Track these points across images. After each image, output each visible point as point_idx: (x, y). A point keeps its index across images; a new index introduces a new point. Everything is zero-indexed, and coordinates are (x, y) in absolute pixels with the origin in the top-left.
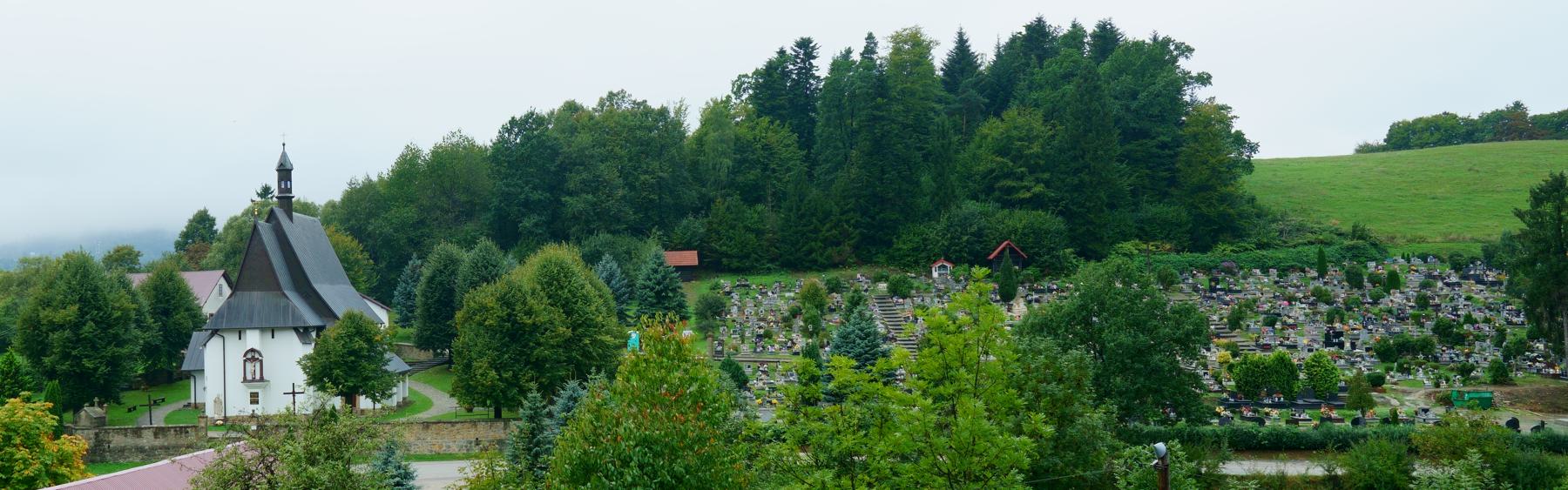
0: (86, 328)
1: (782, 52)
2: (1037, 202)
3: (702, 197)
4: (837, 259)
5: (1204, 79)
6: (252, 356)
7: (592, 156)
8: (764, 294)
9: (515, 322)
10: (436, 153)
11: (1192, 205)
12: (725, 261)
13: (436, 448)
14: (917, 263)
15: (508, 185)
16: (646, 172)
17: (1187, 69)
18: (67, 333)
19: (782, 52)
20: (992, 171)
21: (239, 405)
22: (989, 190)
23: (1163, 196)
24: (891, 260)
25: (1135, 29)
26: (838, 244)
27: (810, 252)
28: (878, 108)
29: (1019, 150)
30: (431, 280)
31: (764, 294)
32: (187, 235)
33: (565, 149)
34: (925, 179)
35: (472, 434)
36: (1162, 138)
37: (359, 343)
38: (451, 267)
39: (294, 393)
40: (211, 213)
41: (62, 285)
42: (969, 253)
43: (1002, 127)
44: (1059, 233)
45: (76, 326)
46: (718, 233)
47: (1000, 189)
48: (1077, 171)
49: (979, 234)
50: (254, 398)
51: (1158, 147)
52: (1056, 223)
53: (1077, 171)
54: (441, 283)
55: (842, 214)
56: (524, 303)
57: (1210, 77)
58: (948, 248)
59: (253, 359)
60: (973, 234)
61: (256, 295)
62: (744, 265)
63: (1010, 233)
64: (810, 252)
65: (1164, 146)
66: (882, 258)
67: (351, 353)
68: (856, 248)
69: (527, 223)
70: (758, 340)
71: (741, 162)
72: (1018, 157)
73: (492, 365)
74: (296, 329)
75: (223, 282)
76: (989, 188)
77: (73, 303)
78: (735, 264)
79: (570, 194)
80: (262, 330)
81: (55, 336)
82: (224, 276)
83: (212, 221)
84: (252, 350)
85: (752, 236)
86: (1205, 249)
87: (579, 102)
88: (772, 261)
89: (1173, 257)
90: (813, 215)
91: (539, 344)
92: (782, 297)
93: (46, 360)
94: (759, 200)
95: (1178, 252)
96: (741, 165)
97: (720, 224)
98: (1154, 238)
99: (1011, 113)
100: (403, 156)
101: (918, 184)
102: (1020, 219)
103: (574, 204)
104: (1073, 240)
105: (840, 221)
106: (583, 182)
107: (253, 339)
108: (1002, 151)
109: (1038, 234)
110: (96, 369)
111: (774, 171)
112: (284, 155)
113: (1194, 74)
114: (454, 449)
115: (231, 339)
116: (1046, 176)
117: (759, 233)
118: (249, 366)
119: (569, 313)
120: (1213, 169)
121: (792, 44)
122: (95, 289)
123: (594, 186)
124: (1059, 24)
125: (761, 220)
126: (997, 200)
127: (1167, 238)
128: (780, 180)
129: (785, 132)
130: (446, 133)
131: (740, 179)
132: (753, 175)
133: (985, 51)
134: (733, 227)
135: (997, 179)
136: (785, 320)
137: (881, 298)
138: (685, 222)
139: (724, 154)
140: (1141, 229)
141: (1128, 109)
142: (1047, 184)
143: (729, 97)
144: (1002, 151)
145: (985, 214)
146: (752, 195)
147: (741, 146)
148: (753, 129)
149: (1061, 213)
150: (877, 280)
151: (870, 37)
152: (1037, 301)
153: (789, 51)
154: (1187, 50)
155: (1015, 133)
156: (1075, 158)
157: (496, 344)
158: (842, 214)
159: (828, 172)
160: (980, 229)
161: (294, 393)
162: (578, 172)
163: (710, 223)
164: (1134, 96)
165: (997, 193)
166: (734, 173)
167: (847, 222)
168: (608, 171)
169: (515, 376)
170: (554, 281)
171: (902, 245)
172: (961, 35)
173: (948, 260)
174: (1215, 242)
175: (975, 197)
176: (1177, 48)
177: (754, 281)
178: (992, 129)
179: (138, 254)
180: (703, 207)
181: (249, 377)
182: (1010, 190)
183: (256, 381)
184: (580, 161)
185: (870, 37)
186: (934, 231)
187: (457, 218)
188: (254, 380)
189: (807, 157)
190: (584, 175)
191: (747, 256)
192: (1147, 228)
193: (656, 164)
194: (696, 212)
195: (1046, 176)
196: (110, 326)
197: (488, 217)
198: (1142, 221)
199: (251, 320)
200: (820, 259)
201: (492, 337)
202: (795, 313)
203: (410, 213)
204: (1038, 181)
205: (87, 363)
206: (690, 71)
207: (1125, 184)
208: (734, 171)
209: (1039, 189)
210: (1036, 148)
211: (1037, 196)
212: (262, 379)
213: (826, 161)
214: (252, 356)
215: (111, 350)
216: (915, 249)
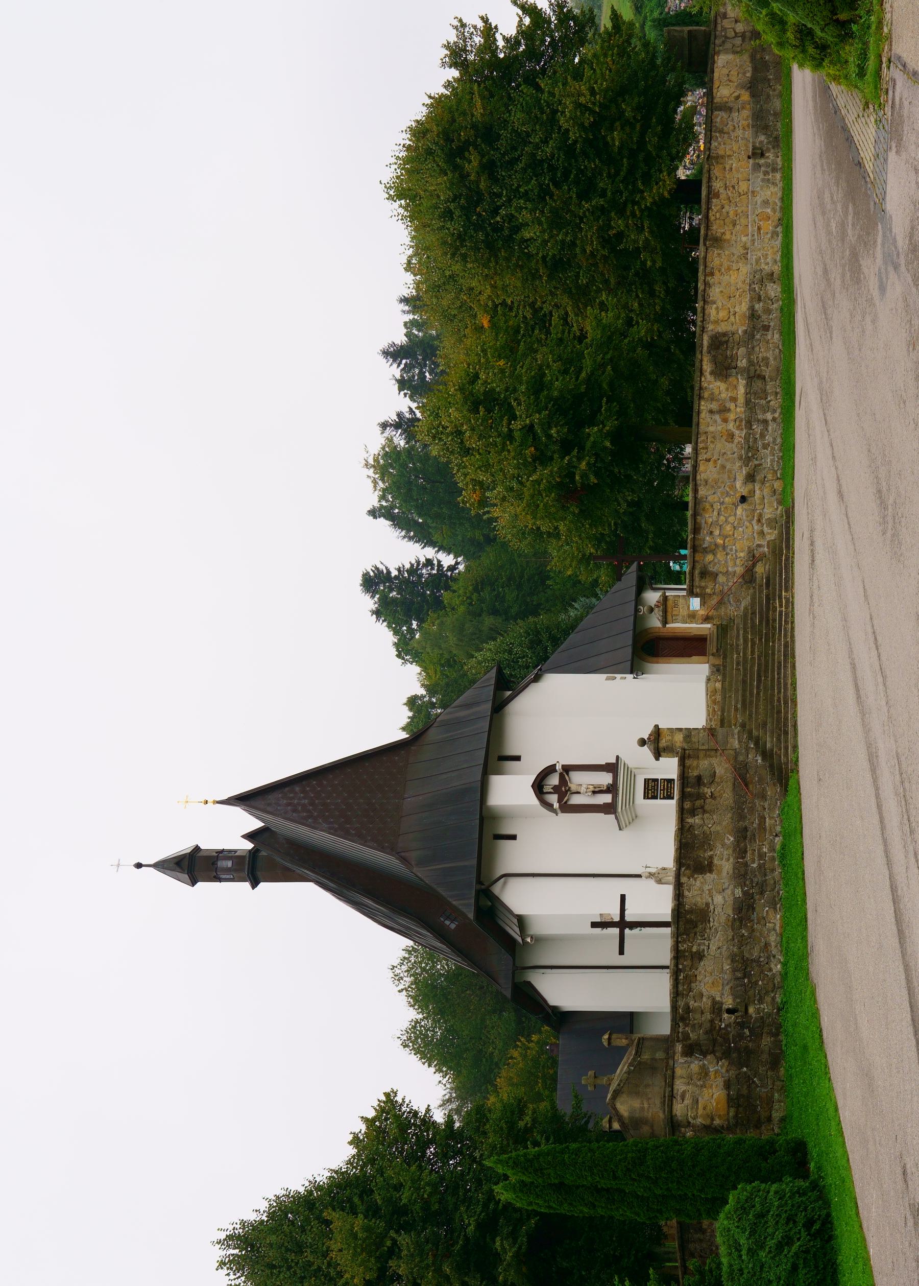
13: (768, 226)
59: (563, 790)
114: (772, 193)
212: (612, 768)
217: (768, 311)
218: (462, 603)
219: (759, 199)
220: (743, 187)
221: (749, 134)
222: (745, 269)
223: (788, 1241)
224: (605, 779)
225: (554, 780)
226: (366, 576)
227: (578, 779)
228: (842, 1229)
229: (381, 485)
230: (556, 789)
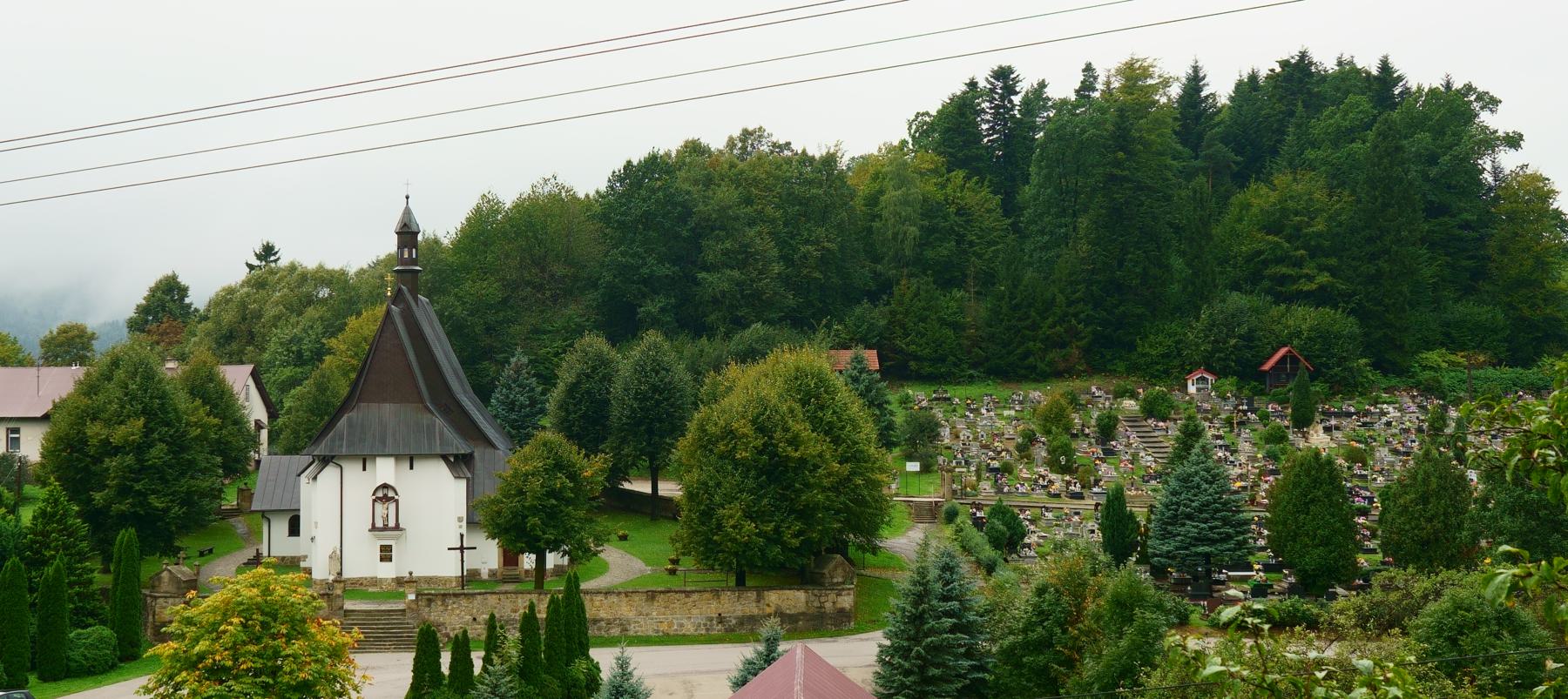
0: (154, 452)
1: (973, 85)
2: (1321, 298)
3: (876, 275)
4: (1062, 366)
5: (1514, 141)
6: (385, 494)
7: (737, 218)
8: (976, 411)
9: (774, 455)
10: (518, 206)
11: (1510, 305)
12: (913, 365)
13: (664, 627)
14: (1167, 373)
15: (623, 254)
16: (807, 242)
17: (1492, 127)
18: (130, 459)
19: (973, 85)
20: (1260, 253)
21: (362, 563)
22: (1255, 278)
23: (1467, 291)
24: (1133, 369)
25: (1421, 72)
26: (1063, 345)
27: (1026, 355)
28: (1118, 164)
29: (1298, 228)
30: (572, 389)
31: (976, 411)
32: (144, 310)
33: (701, 207)
34: (1177, 263)
35: (712, 608)
36: (1466, 216)
37: (561, 481)
38: (602, 371)
39: (462, 549)
40: (183, 280)
41: (113, 390)
42: (1237, 362)
43: (1274, 197)
44: (1352, 337)
45: (140, 449)
46: (903, 326)
47: (1272, 278)
48: (1373, 257)
49: (1249, 338)
50: (386, 554)
51: (1461, 227)
52: (1347, 325)
53: (1373, 257)
54: (588, 392)
55: (1070, 304)
56: (786, 430)
57: (1521, 136)
58: (1212, 354)
59: (386, 499)
60: (1241, 337)
61: (388, 408)
62: (939, 370)
63: (1291, 336)
64: (1026, 355)
65: (1466, 226)
66: (1121, 366)
67: (552, 493)
68: (1087, 351)
69: (651, 307)
70: (1003, 484)
71: (930, 230)
72: (1295, 236)
73: (748, 516)
74: (445, 458)
75: (251, 382)
76: (1253, 275)
77: (137, 415)
78: (927, 369)
79: (706, 268)
80: (398, 458)
81: (112, 463)
82: (255, 375)
83: (183, 291)
84: (385, 486)
85: (949, 332)
86: (1527, 364)
87: (704, 141)
88: (974, 366)
89: (1490, 371)
90: (1030, 305)
91: (808, 486)
92: (1000, 416)
93: (98, 497)
94: (960, 283)
95: (1494, 366)
96: (930, 234)
97: (907, 313)
98: (1462, 347)
99: (1282, 179)
100: (478, 210)
101: (1167, 268)
102: (1304, 317)
103: (716, 282)
104: (1368, 348)
105: (1066, 314)
106: (726, 253)
107: (385, 470)
108: (1273, 228)
109: (1324, 337)
110: (166, 510)
111: (971, 244)
112: (407, 212)
113: (1501, 133)
114: (689, 628)
115: (352, 470)
116: (1333, 261)
117: (956, 326)
118: (379, 506)
119: (836, 441)
120: (1537, 258)
121: (987, 73)
122: (163, 396)
123: (743, 257)
124: (1326, 60)
125: (961, 310)
126: (1268, 292)
127: (1480, 347)
128: (979, 256)
129: (985, 192)
130: (536, 179)
131: (929, 254)
132: (946, 249)
133: (1221, 87)
134: (923, 320)
135: (1265, 263)
136: (1020, 448)
137: (1132, 420)
138: (858, 311)
139: (907, 219)
140: (1447, 335)
141: (1426, 178)
142: (1333, 272)
143: (904, 143)
144: (1273, 228)
145: (1256, 311)
146: (948, 277)
147: (930, 210)
148: (943, 187)
149: (1352, 312)
150: (1120, 394)
151: (1088, 68)
152: (1337, 428)
153: (982, 84)
154: (1491, 103)
155: (1291, 204)
156: (1370, 240)
157: (750, 483)
158: (1070, 304)
159: (1045, 248)
160: (1251, 331)
161: (462, 549)
162: (718, 240)
163: (893, 313)
164: (1433, 160)
165: (1266, 283)
166: (920, 246)
167: (1076, 315)
168: (760, 240)
169: (777, 530)
170: (811, 394)
171: (1152, 347)
172: (1196, 69)
173: (1210, 370)
174: (1539, 355)
175: (1236, 287)
176: (1480, 97)
177: (957, 393)
178: (1260, 197)
179: (93, 337)
180: (881, 290)
181: (379, 524)
182: (1282, 280)
183: (387, 531)
184: (721, 224)
185: (1088, 68)
186: (1194, 333)
187: (555, 298)
188: (386, 528)
189: (1015, 227)
190: (728, 245)
191: (943, 360)
192: (1454, 333)
193: (820, 232)
194: (873, 297)
195: (1333, 261)
196: (183, 449)
197: (592, 297)
198: (1448, 325)
199: (383, 442)
200: (1041, 366)
201: (745, 475)
202: (1030, 439)
203: (490, 289)
204: (1321, 268)
205: (156, 502)
206: (855, 108)
207: (1427, 272)
208: (922, 244)
209: (1324, 278)
210: (1319, 226)
211: (1322, 288)
212: (397, 527)
213: (1042, 232)
214: (385, 494)
215: (185, 484)
216: (1165, 356)
217: (599, 629)
218: (946, 196)
219: (684, 621)
220: (695, 611)
221: (739, 613)
222: (631, 615)
223: (86, 658)
224: (392, 524)
225: (391, 494)
226: (1010, 70)
227: (392, 506)
228: (89, 681)
229: (892, 194)
230: (385, 496)
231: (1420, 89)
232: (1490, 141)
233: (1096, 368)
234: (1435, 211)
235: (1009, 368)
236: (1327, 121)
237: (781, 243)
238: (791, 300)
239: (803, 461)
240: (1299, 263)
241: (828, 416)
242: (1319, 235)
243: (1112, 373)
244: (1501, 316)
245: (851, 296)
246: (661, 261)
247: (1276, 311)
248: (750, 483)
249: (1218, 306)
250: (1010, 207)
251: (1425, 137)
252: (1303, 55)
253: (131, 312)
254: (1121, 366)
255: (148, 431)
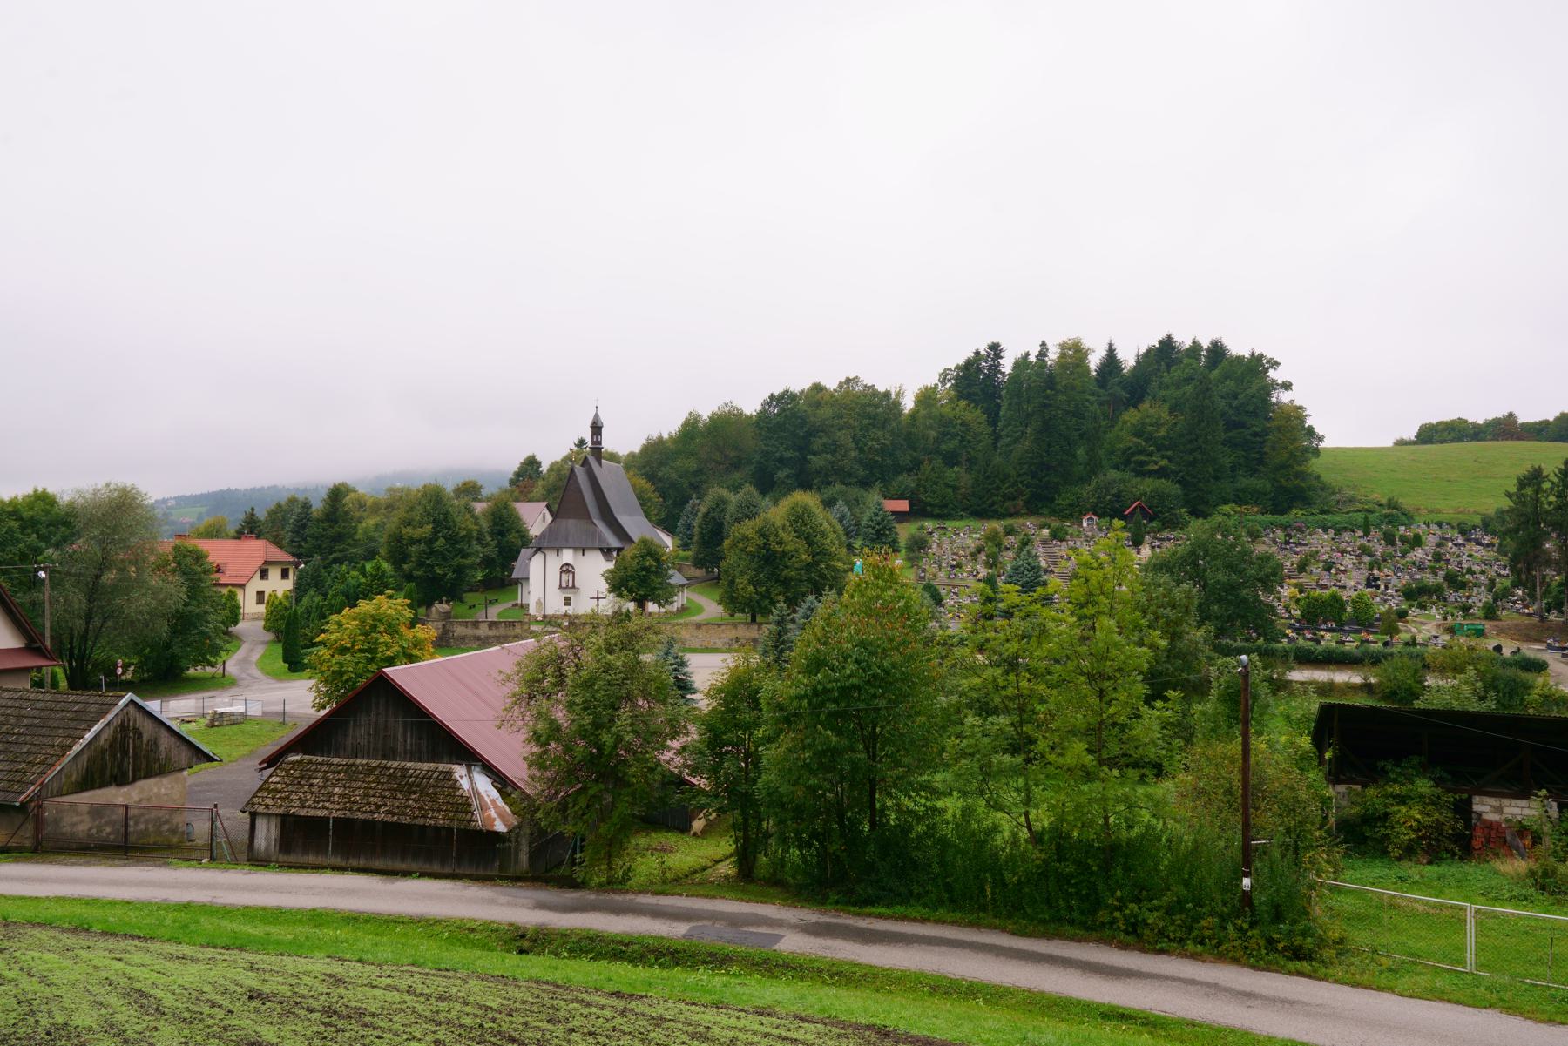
1: (977, 353)
2: (1162, 473)
5: (1287, 386)
6: (567, 569)
18: (423, 546)
19: (977, 353)
21: (555, 606)
22: (1127, 462)
23: (1253, 472)
24: (1053, 512)
25: (1238, 348)
27: (993, 503)
28: (1047, 397)
30: (706, 515)
32: (517, 474)
37: (650, 562)
40: (538, 458)
43: (1139, 415)
44: (1177, 497)
45: (430, 541)
48: (1192, 451)
49: (1118, 496)
50: (567, 601)
52: (1176, 489)
53: (1192, 451)
59: (568, 571)
61: (571, 521)
64: (993, 503)
65: (1256, 434)
66: (1046, 511)
67: (644, 569)
68: (1027, 502)
71: (944, 434)
73: (751, 582)
74: (601, 550)
78: (937, 511)
80: (575, 549)
81: (413, 548)
83: (539, 464)
86: (1282, 513)
89: (1259, 517)
94: (958, 464)
100: (687, 421)
101: (1074, 456)
102: (1149, 485)
103: (817, 462)
106: (824, 445)
107: (568, 556)
112: (597, 415)
114: (719, 644)
115: (551, 555)
116: (1169, 453)
117: (955, 488)
119: (810, 544)
122: (447, 513)
123: (834, 448)
124: (1184, 340)
127: (1256, 503)
130: (721, 404)
133: (1128, 359)
135: (1133, 454)
136: (972, 555)
137: (1044, 541)
145: (1123, 481)
146: (951, 460)
149: (1179, 482)
150: (1042, 527)
151: (1043, 344)
156: (1191, 441)
157: (754, 565)
164: (1236, 397)
168: (844, 437)
170: (800, 519)
171: (1062, 502)
172: (1111, 345)
173: (1095, 513)
174: (1290, 508)
175: (1116, 467)
178: (1131, 417)
180: (914, 467)
182: (1142, 463)
185: (1043, 344)
186: (1087, 492)
191: (946, 506)
193: (880, 434)
194: (909, 470)
195: (1169, 453)
196: (457, 542)
202: (980, 550)
203: (692, 465)
204: (1163, 457)
205: (438, 571)
206: (907, 364)
207: (1227, 461)
208: (938, 441)
209: (1164, 463)
210: (1162, 432)
211: (1162, 468)
214: (567, 569)
215: (458, 560)
231: (1196, 346)
232: (1274, 385)
233: (1032, 511)
234: (1232, 425)
235: (982, 513)
236: (1177, 373)
237: (856, 441)
238: (861, 472)
239: (784, 554)
240: (1151, 454)
241: (808, 529)
242: (1163, 438)
243: (1042, 515)
244: (1269, 486)
245: (898, 470)
246: (787, 449)
247: (1134, 481)
248: (754, 565)
249: (1102, 477)
250: (993, 419)
251: (1231, 384)
252: (1169, 337)
253: (511, 476)
254: (1046, 511)
255: (435, 532)
